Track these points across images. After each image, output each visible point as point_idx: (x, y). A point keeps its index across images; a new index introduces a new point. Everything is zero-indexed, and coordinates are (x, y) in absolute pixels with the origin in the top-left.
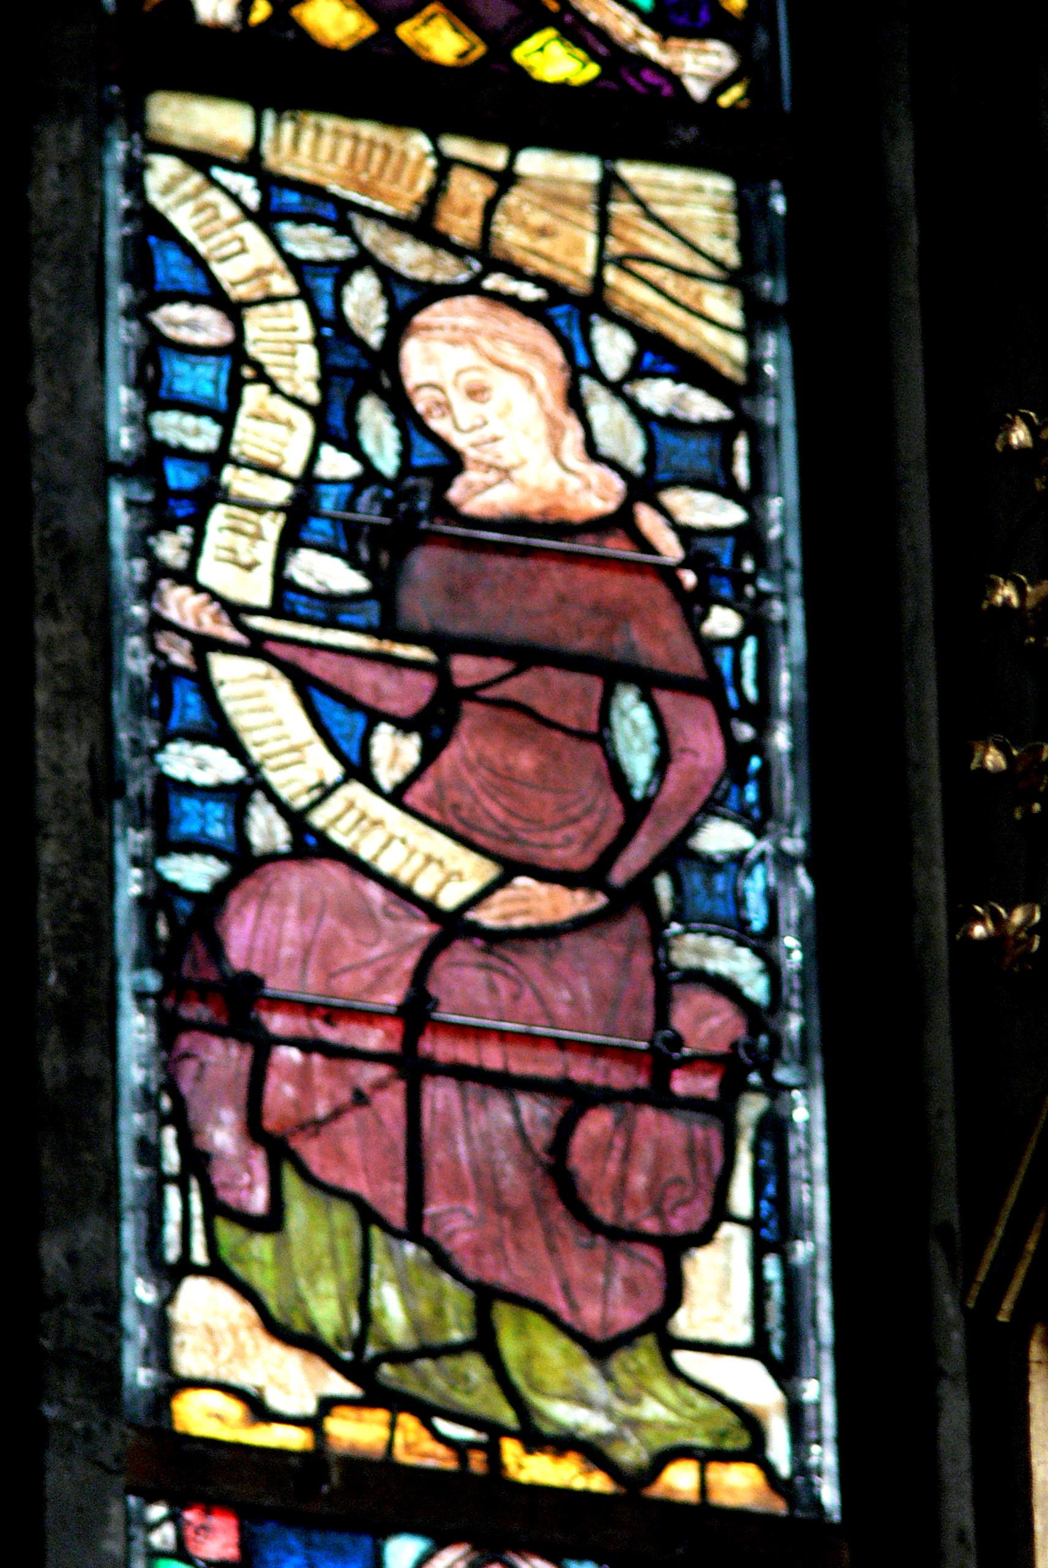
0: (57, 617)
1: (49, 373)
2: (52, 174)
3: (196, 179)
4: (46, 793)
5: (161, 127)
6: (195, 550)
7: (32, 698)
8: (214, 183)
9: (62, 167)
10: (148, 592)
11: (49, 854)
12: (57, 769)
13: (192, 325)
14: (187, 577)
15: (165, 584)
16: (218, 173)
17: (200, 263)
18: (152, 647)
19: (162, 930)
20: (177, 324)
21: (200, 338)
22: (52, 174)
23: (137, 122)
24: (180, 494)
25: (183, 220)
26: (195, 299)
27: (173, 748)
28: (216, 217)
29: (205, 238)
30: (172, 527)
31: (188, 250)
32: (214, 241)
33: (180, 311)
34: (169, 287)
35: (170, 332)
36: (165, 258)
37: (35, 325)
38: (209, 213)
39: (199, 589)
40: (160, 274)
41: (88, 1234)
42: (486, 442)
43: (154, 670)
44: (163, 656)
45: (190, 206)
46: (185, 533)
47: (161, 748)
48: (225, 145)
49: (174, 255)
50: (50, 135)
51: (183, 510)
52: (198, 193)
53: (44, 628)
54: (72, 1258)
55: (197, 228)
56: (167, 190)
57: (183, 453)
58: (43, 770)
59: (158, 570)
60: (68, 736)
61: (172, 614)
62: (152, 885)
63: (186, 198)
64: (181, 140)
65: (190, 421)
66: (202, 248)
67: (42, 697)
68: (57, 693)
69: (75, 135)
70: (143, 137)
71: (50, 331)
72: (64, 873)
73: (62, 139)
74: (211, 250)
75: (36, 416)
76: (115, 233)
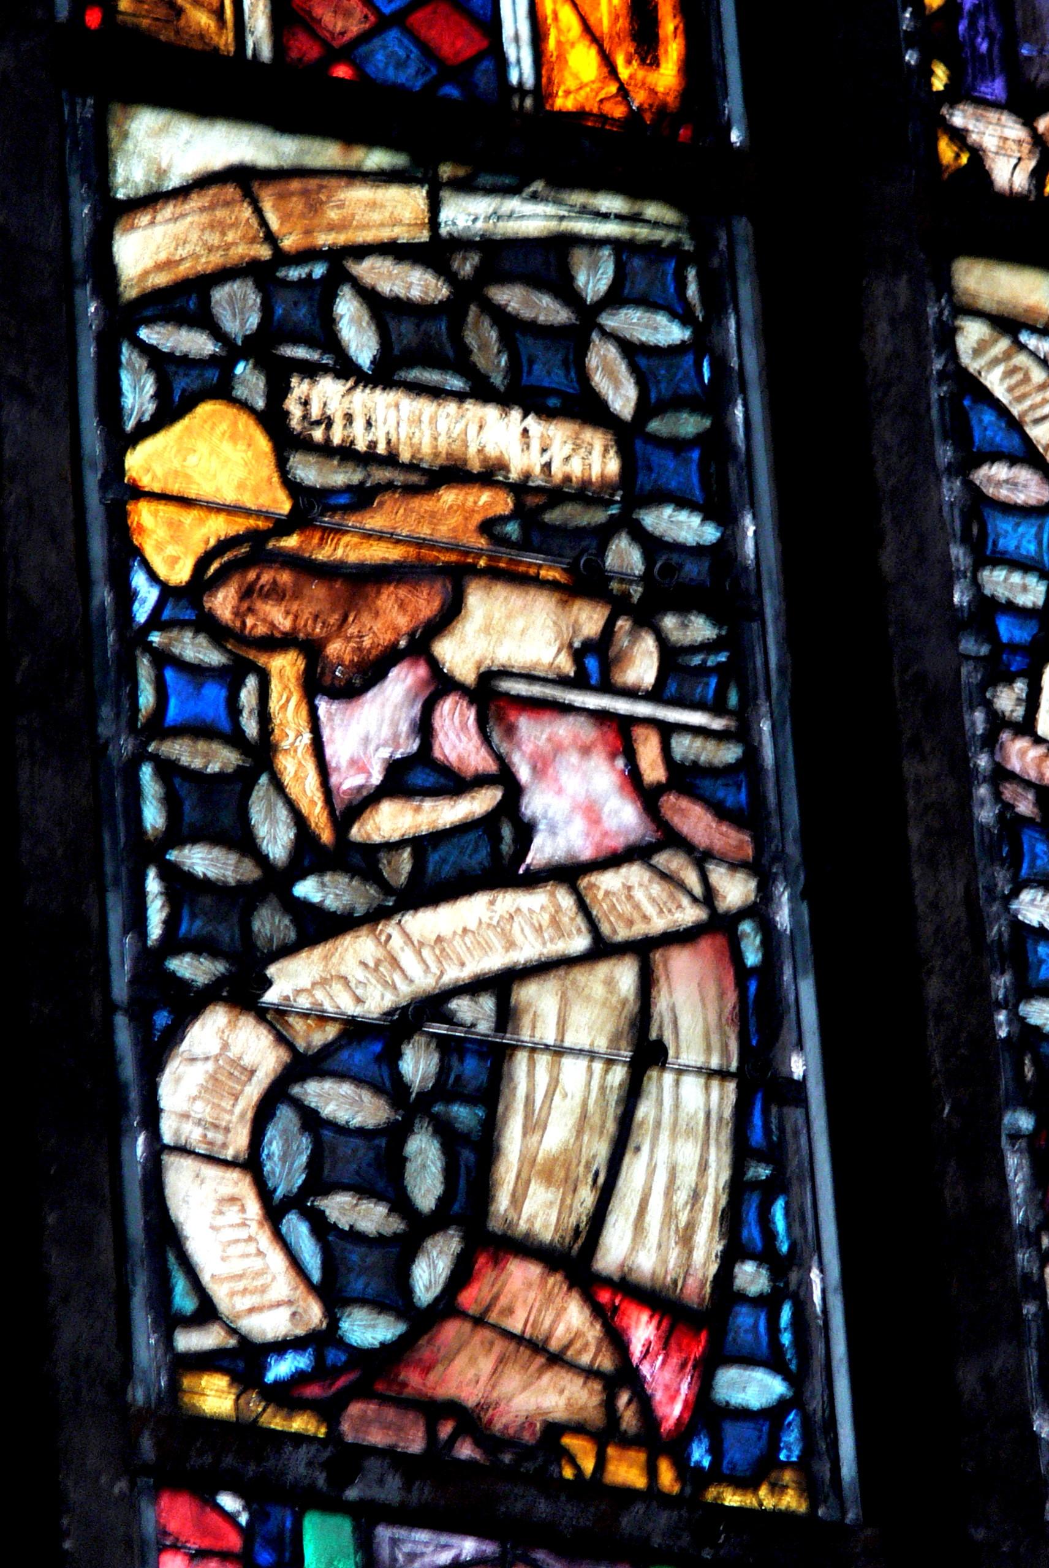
0: (923, 759)
1: (896, 520)
2: (883, 328)
3: (1004, 344)
4: (926, 929)
5: (966, 292)
6: (1032, 702)
7: (906, 840)
8: (1022, 347)
9: (892, 322)
10: (990, 741)
11: (934, 988)
12: (934, 906)
13: (1012, 483)
14: (1027, 727)
15: (1005, 736)
16: (1024, 337)
17: (1015, 425)
18: (997, 796)
19: (1029, 1073)
20: (999, 484)
21: (1020, 498)
22: (883, 328)
23: (945, 284)
24: (1013, 648)
25: (995, 382)
26: (1013, 460)
27: (1026, 896)
28: (1027, 379)
29: (1020, 399)
30: (1009, 681)
31: (1002, 411)
32: (1027, 403)
33: (1000, 471)
34: (987, 448)
35: (990, 491)
36: (981, 421)
37: (880, 472)
38: (1018, 376)
39: (1038, 740)
40: (977, 434)
41: (1001, 1360)
42: (198, 1155)
43: (1000, 818)
44: (1008, 807)
45: (999, 370)
46: (1020, 687)
47: (1015, 893)
48: (1029, 310)
49: (989, 417)
50: (879, 289)
51: (1018, 663)
52: (1007, 356)
53: (912, 768)
54: (986, 1381)
55: (1010, 390)
56: (978, 352)
57: (1011, 608)
58: (921, 908)
59: (998, 722)
60: (944, 874)
61: (1015, 764)
62: (1016, 1029)
63: (995, 362)
64: (989, 306)
65: (1016, 578)
66: (1016, 411)
67: (915, 836)
68: (928, 833)
69: (902, 289)
70: (950, 301)
71: (893, 481)
72: (949, 1007)
73: (890, 294)
74: (1025, 413)
75: (888, 561)
76: (937, 392)
